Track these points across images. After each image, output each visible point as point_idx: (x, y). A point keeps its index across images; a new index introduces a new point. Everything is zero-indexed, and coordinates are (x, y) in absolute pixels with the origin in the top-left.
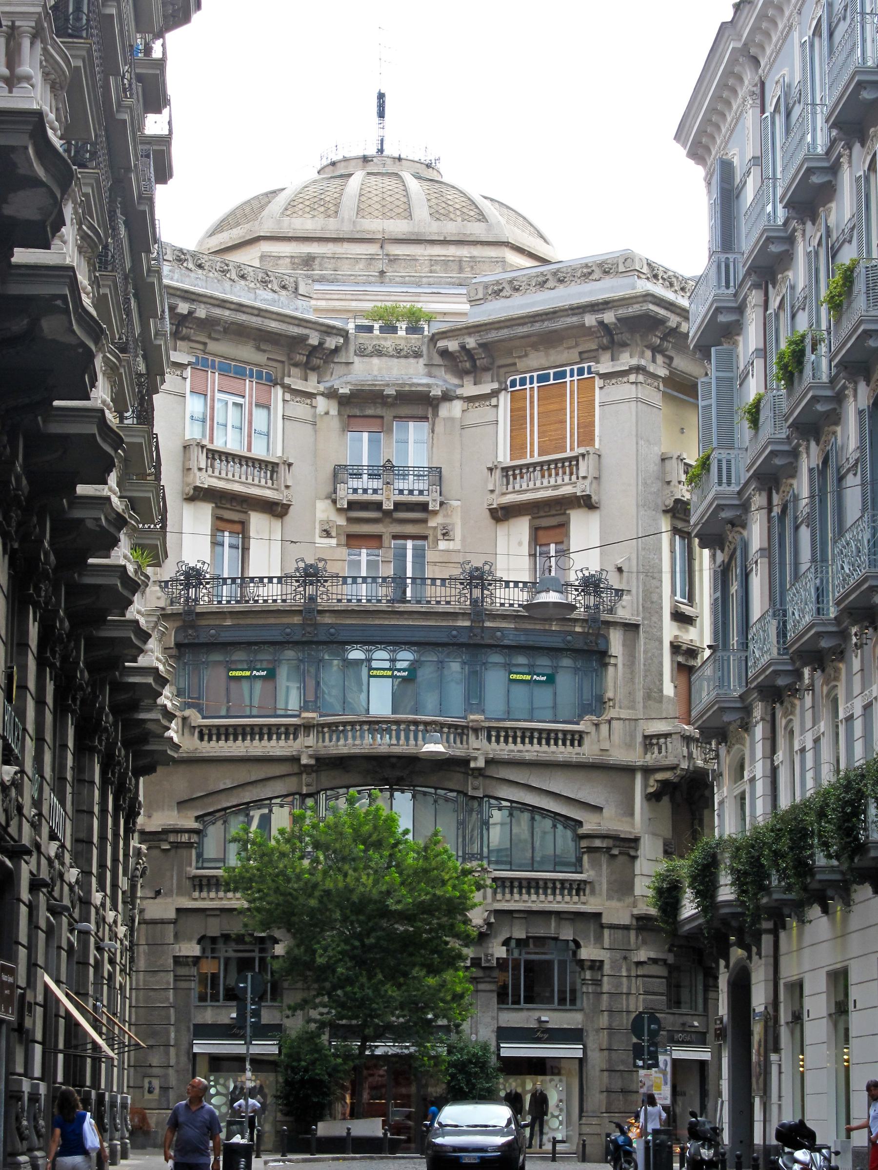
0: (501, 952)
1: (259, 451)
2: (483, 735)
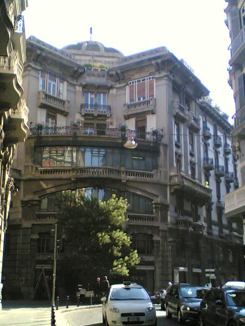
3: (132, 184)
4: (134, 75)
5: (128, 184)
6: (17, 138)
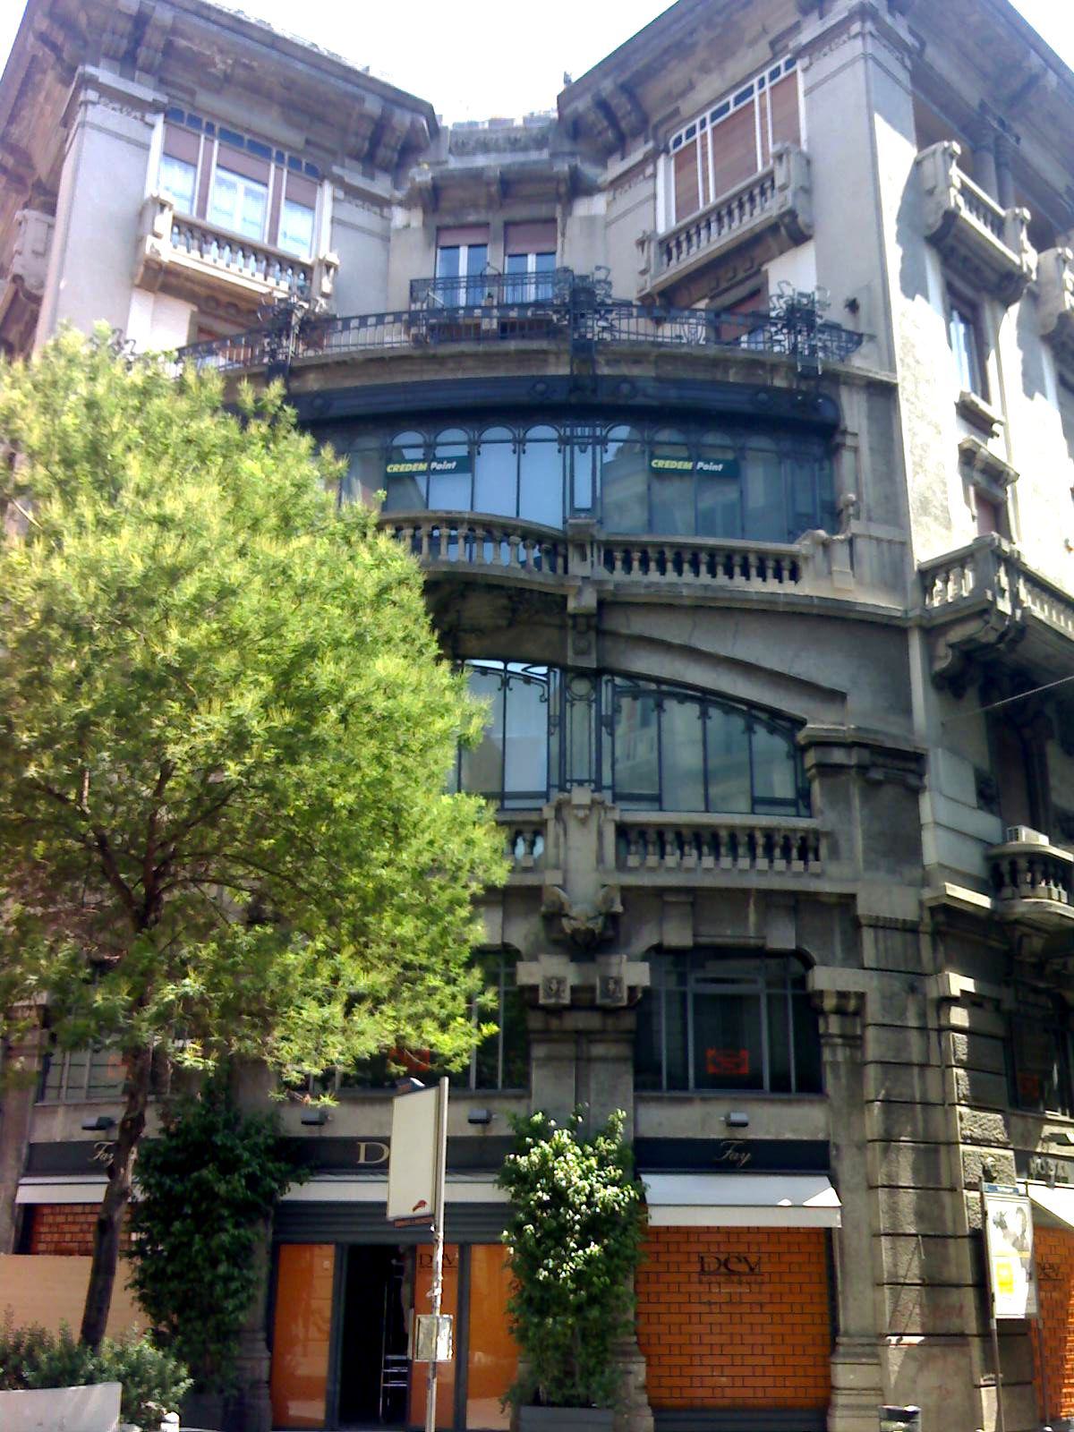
0: (636, 974)
2: (596, 556)
4: (691, 86)
5: (616, 622)
6: (980, 808)
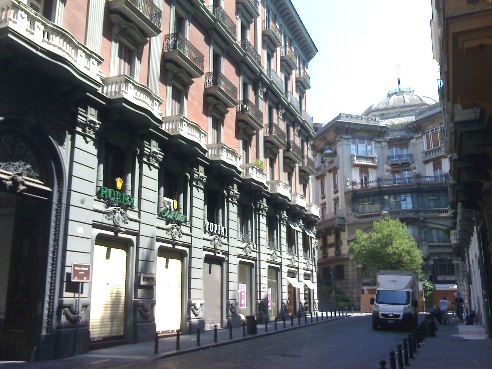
0: (432, 263)
1: (369, 155)
2: (423, 212)
3: (429, 220)
4: (428, 126)
